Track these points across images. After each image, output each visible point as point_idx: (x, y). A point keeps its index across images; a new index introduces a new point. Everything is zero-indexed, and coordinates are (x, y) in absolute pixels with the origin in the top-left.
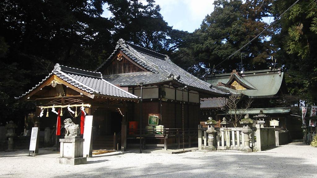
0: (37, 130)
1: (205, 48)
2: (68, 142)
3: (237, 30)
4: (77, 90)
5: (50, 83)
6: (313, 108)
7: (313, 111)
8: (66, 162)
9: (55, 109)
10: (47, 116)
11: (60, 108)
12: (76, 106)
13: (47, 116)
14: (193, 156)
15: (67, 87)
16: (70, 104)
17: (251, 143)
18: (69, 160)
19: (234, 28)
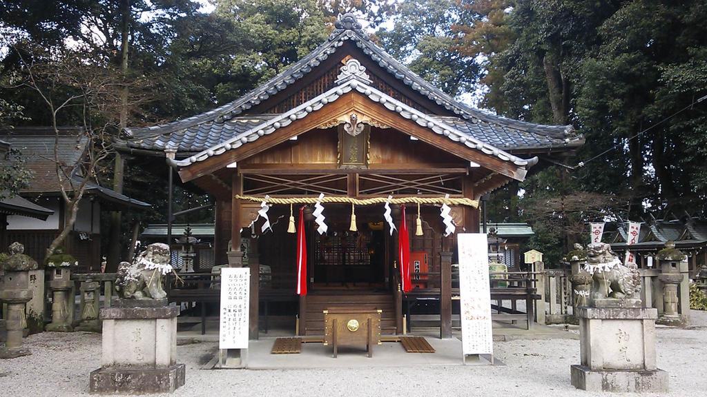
0: (249, 275)
1: (240, 70)
2: (619, 319)
3: (319, 38)
4: (457, 153)
5: (335, 120)
6: (633, 227)
7: (633, 233)
8: (633, 383)
9: (322, 209)
10: (289, 231)
11: (349, 205)
12: (418, 200)
13: (289, 231)
14: (224, 333)
15: (412, 138)
16: (327, 192)
17: (514, 304)
18: (646, 379)
19: (312, 32)
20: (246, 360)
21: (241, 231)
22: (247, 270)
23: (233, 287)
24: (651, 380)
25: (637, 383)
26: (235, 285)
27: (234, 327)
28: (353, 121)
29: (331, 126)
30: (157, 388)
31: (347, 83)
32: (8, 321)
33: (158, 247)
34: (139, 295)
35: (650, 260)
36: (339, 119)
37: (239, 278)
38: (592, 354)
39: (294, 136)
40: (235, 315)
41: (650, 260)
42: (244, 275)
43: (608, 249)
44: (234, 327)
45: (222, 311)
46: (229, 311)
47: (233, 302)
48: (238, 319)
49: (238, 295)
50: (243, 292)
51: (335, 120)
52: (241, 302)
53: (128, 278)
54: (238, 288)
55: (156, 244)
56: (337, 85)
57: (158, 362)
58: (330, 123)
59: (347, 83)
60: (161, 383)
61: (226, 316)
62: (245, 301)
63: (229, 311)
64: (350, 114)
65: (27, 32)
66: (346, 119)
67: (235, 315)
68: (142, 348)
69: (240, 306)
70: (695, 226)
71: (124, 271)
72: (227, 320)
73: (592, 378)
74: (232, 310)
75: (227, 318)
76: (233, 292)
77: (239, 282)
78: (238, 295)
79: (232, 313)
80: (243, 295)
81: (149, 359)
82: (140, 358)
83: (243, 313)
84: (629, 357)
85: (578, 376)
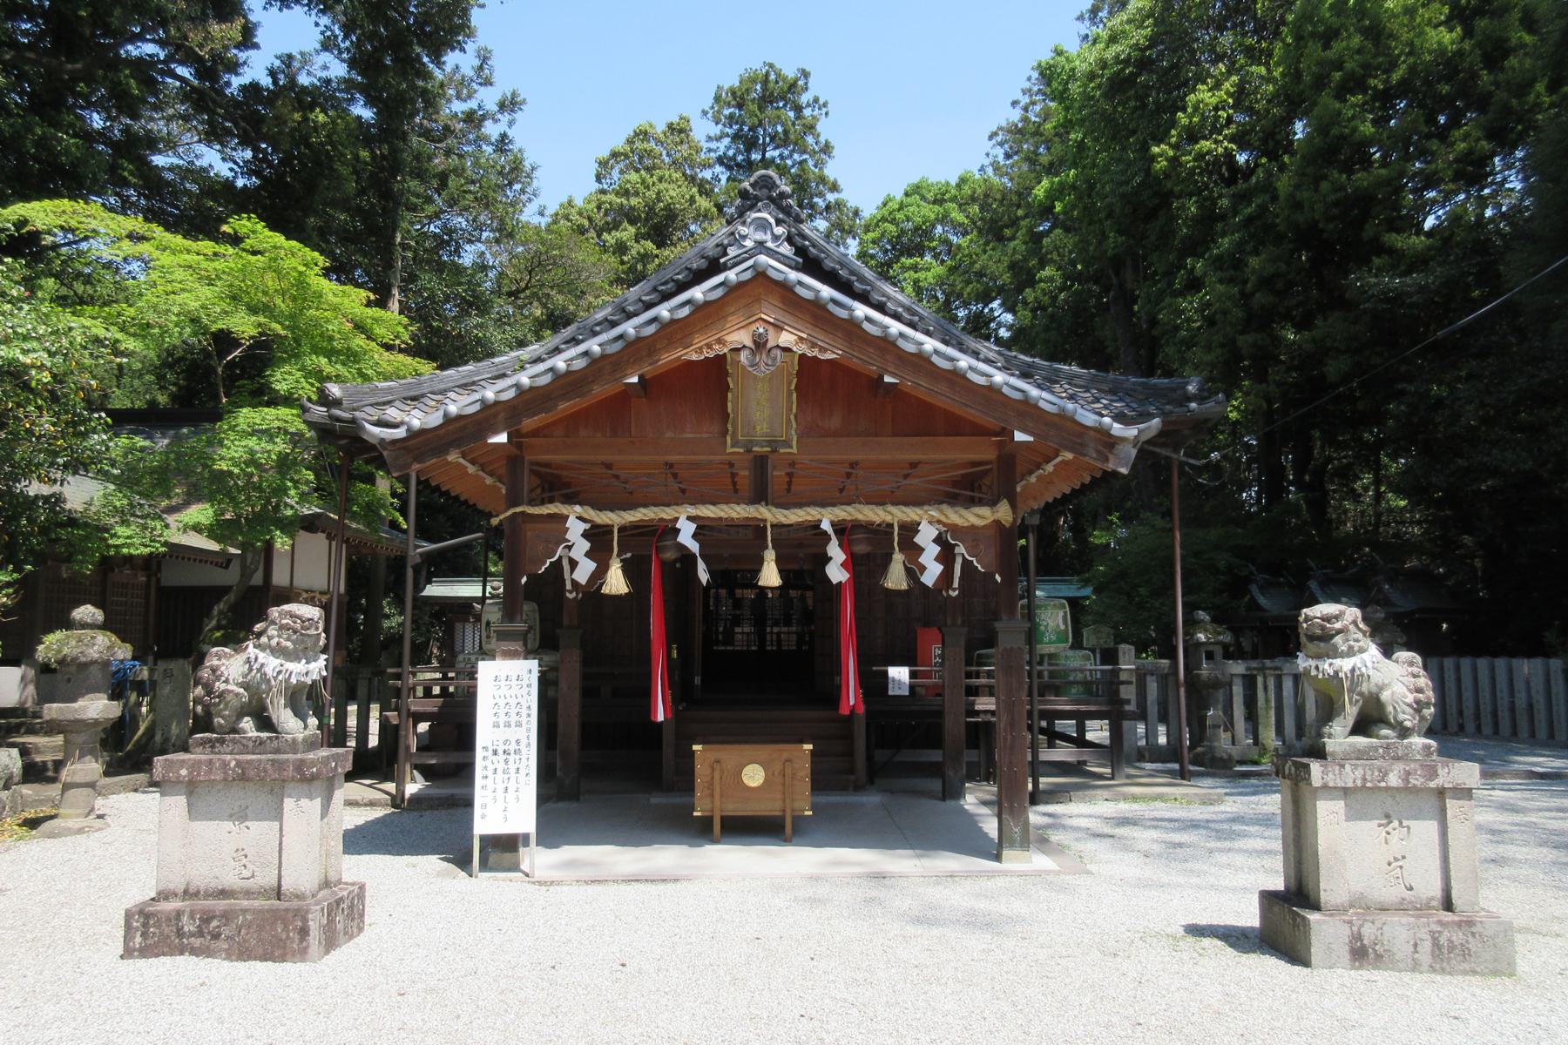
5: (720, 341)
8: (1427, 946)
11: (757, 530)
20: (536, 858)
21: (524, 580)
22: (533, 664)
23: (502, 702)
24: (1470, 939)
25: (1436, 944)
26: (507, 696)
27: (505, 791)
28: (759, 344)
29: (711, 355)
30: (275, 951)
31: (751, 262)
32: (997, 625)
33: (293, 616)
34: (247, 724)
35: (770, 576)
36: (729, 338)
37: (514, 682)
38: (1322, 871)
39: (631, 375)
40: (506, 761)
41: (770, 576)
42: (525, 676)
43: (1355, 622)
44: (505, 791)
45: (479, 753)
46: (495, 752)
47: (502, 734)
48: (513, 771)
49: (513, 719)
50: (524, 712)
51: (720, 341)
52: (521, 734)
53: (223, 686)
54: (513, 702)
55: (286, 607)
56: (725, 268)
57: (287, 885)
58: (709, 346)
59: (751, 262)
60: (288, 937)
61: (488, 763)
62: (529, 730)
63: (495, 752)
64: (754, 327)
65: (63, 165)
66: (742, 337)
67: (506, 761)
68: (250, 851)
69: (518, 742)
70: (1262, 589)
71: (214, 670)
72: (490, 773)
73: (1324, 930)
74: (500, 752)
75: (491, 768)
76: (502, 712)
77: (515, 690)
78: (513, 719)
79: (502, 757)
80: (524, 719)
81: (267, 878)
82: (246, 873)
83: (524, 757)
84: (1409, 880)
85: (1283, 925)
